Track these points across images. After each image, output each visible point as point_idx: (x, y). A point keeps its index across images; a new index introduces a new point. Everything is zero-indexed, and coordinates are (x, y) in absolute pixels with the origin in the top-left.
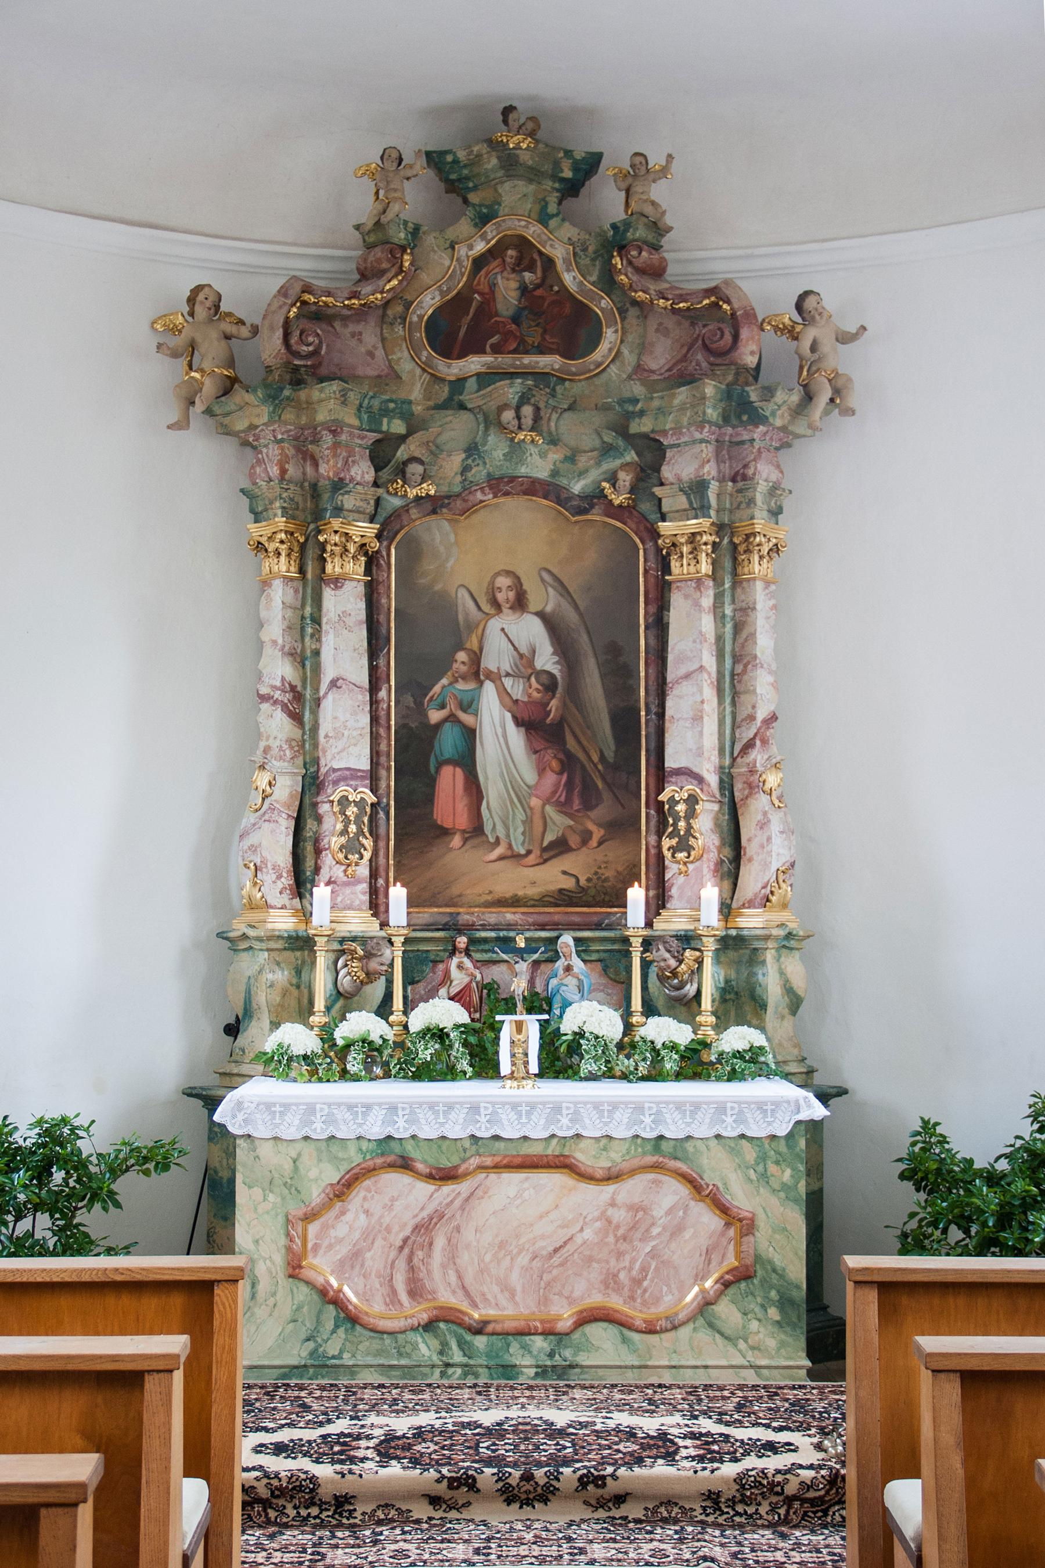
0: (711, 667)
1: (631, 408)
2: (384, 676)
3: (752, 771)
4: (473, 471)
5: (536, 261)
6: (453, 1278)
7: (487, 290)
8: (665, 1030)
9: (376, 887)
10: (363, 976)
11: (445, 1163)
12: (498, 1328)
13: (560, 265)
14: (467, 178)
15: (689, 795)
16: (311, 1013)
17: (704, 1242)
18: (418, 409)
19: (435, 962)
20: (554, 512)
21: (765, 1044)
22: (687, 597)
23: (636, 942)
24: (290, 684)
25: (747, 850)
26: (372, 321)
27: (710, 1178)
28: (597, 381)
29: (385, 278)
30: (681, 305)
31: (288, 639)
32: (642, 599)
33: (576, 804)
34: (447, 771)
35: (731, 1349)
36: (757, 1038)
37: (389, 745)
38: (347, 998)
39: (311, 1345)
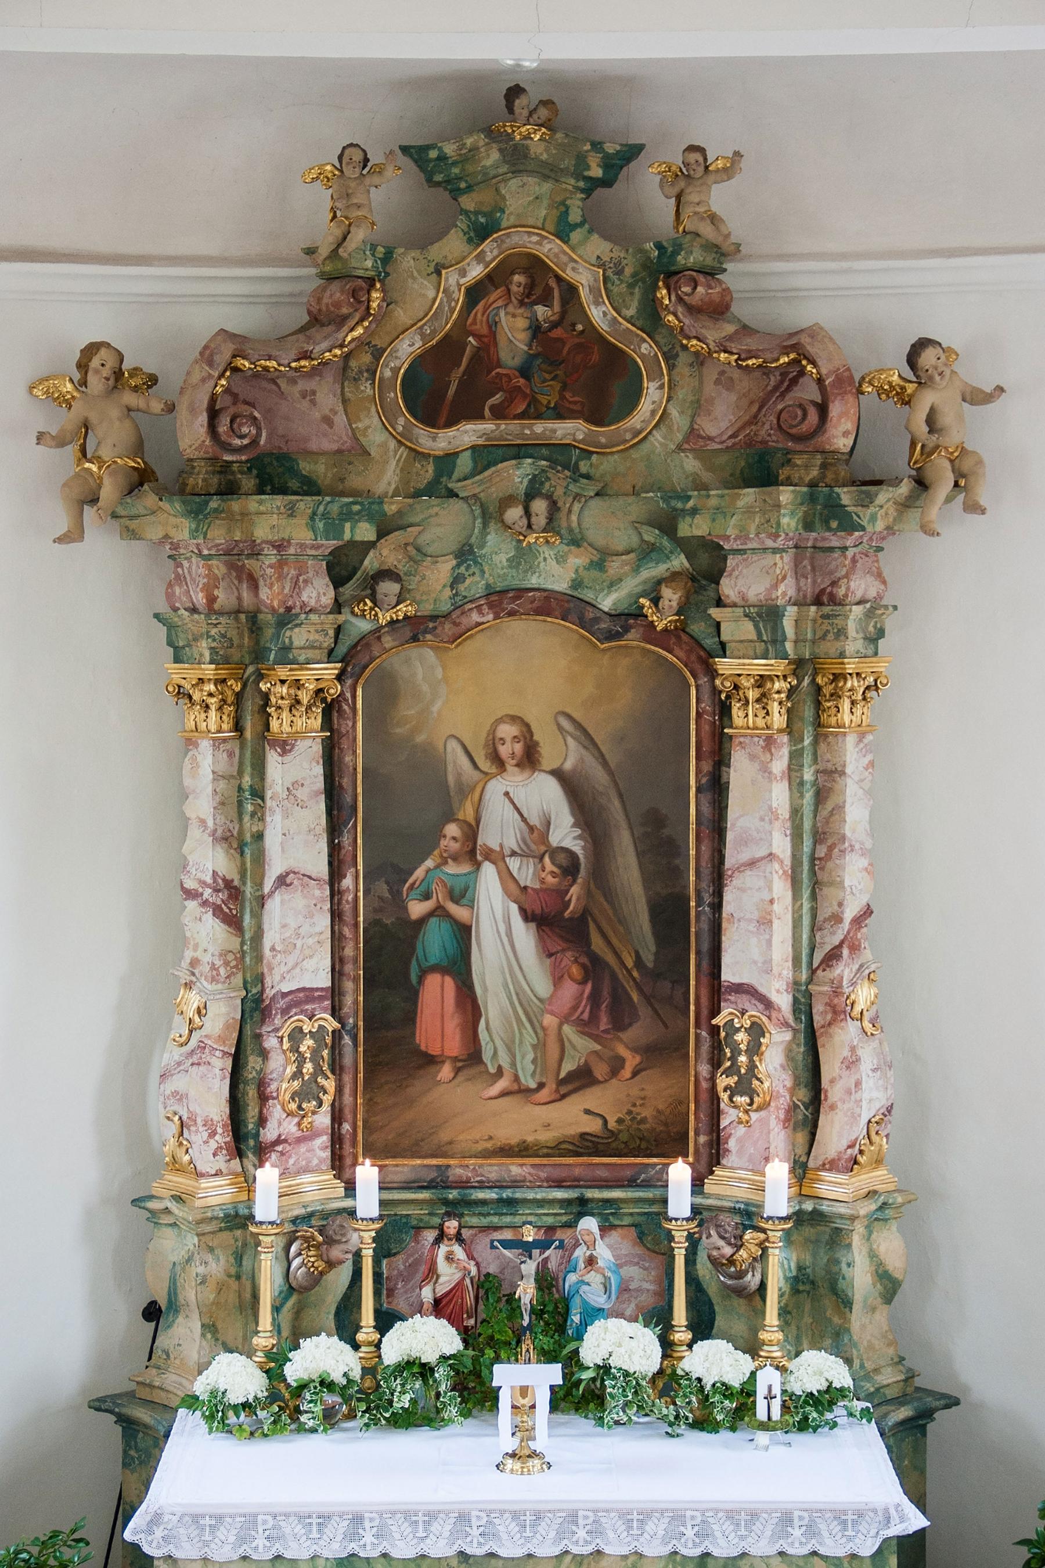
0: (783, 851)
1: (680, 505)
2: (349, 859)
3: (837, 992)
4: (468, 582)
5: (551, 289)
7: (484, 330)
9: (340, 1134)
13: (584, 293)
15: (753, 1024)
20: (576, 637)
22: (753, 757)
24: (224, 880)
25: (829, 1095)
26: (329, 377)
28: (635, 454)
29: (346, 329)
30: (750, 362)
31: (221, 819)
32: (693, 752)
33: (604, 1023)
34: (433, 981)
37: (357, 948)
38: (300, 1293)
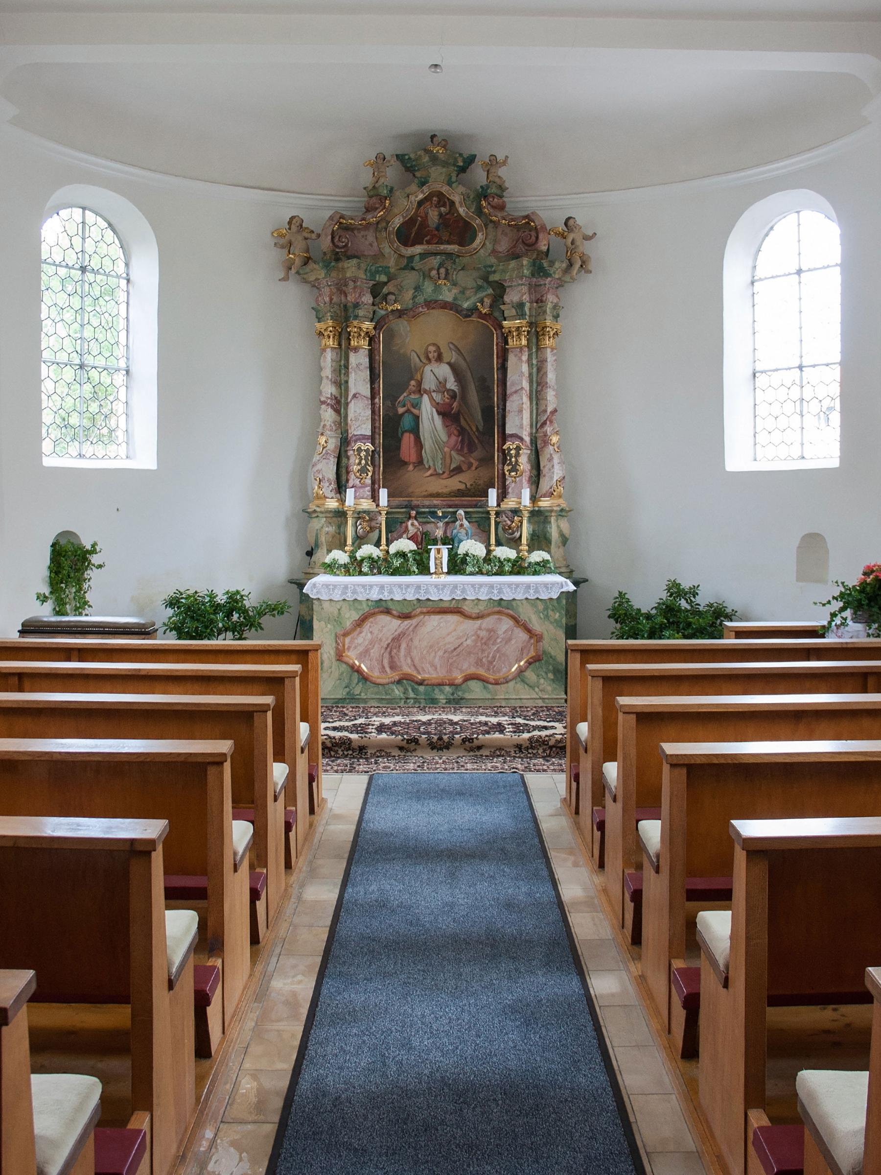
3: (546, 435)
6: (409, 661)
8: (505, 553)
10: (368, 529)
11: (406, 611)
12: (430, 682)
13: (457, 204)
14: (415, 166)
16: (345, 545)
17: (520, 645)
18: (392, 270)
19: (401, 523)
21: (549, 558)
22: (516, 356)
23: (493, 513)
26: (372, 230)
27: (523, 617)
33: (466, 450)
34: (406, 435)
35: (531, 691)
36: (547, 556)
39: (347, 690)
